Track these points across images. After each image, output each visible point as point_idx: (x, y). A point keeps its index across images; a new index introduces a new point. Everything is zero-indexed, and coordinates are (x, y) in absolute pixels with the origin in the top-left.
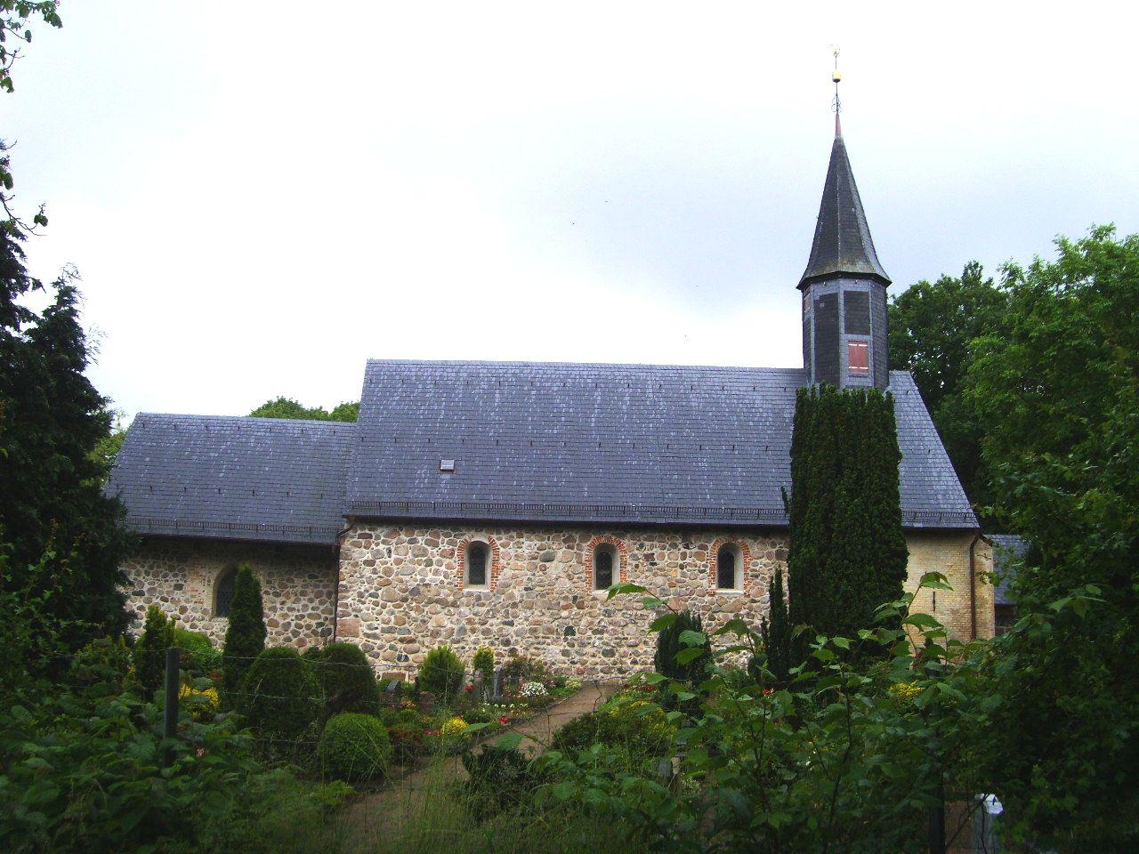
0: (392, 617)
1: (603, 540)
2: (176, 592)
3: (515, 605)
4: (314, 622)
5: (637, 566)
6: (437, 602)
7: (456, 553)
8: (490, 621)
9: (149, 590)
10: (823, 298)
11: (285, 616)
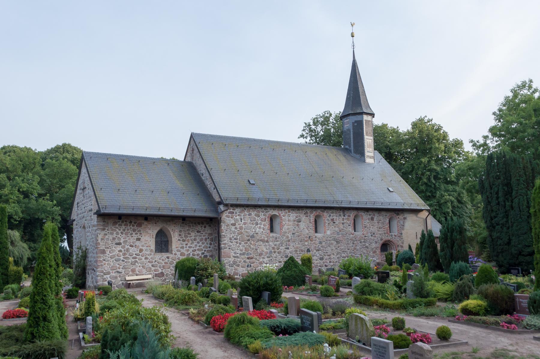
0: (244, 248)
1: (318, 213)
2: (137, 242)
4: (200, 253)
5: (329, 224)
6: (261, 240)
7: (267, 219)
8: (281, 248)
9: (124, 242)
10: (356, 122)
11: (188, 250)
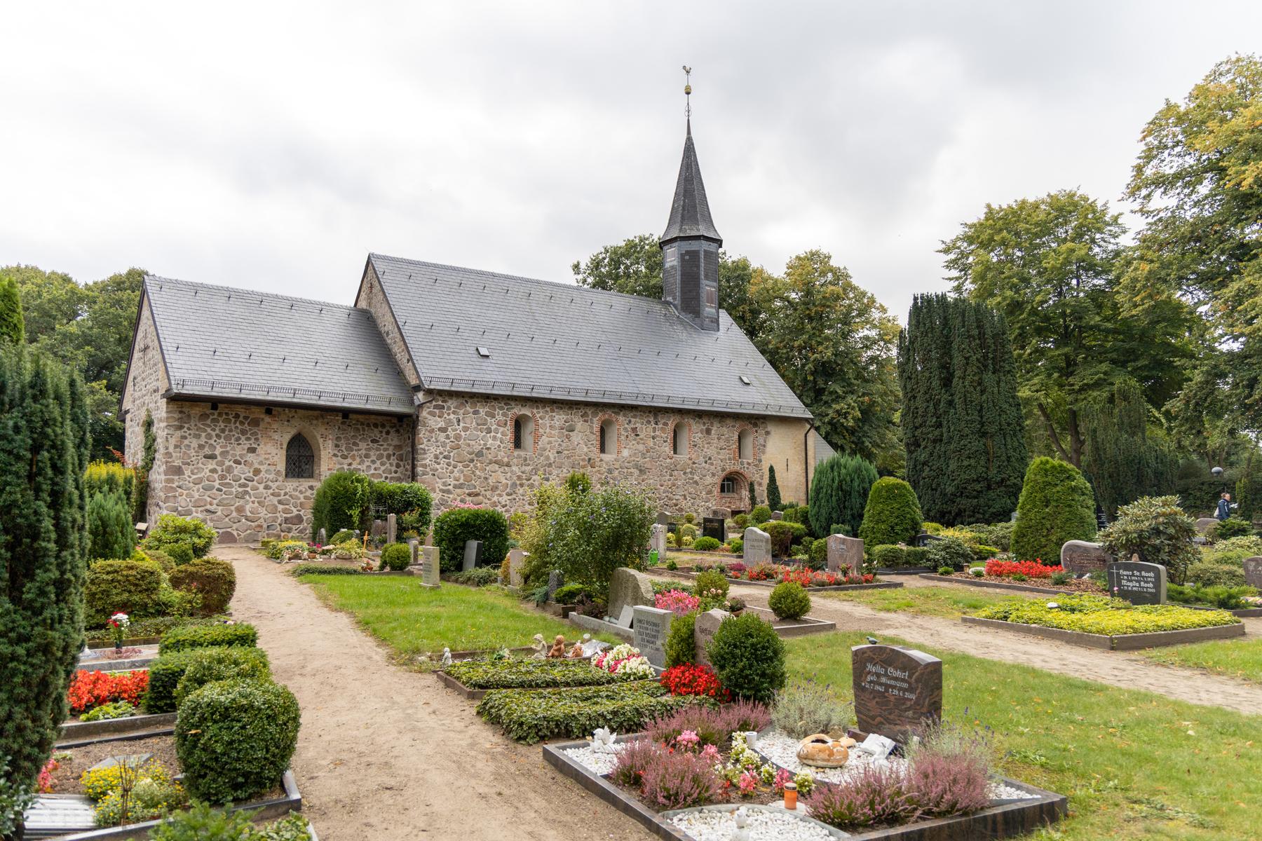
3: (550, 465)
6: (496, 462)
9: (222, 453)
10: (688, 252)
